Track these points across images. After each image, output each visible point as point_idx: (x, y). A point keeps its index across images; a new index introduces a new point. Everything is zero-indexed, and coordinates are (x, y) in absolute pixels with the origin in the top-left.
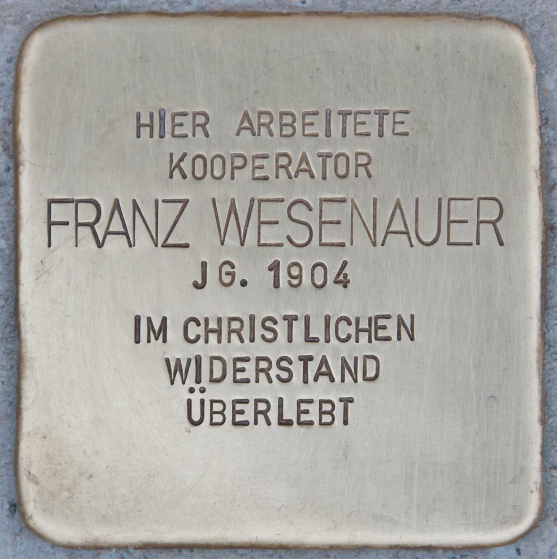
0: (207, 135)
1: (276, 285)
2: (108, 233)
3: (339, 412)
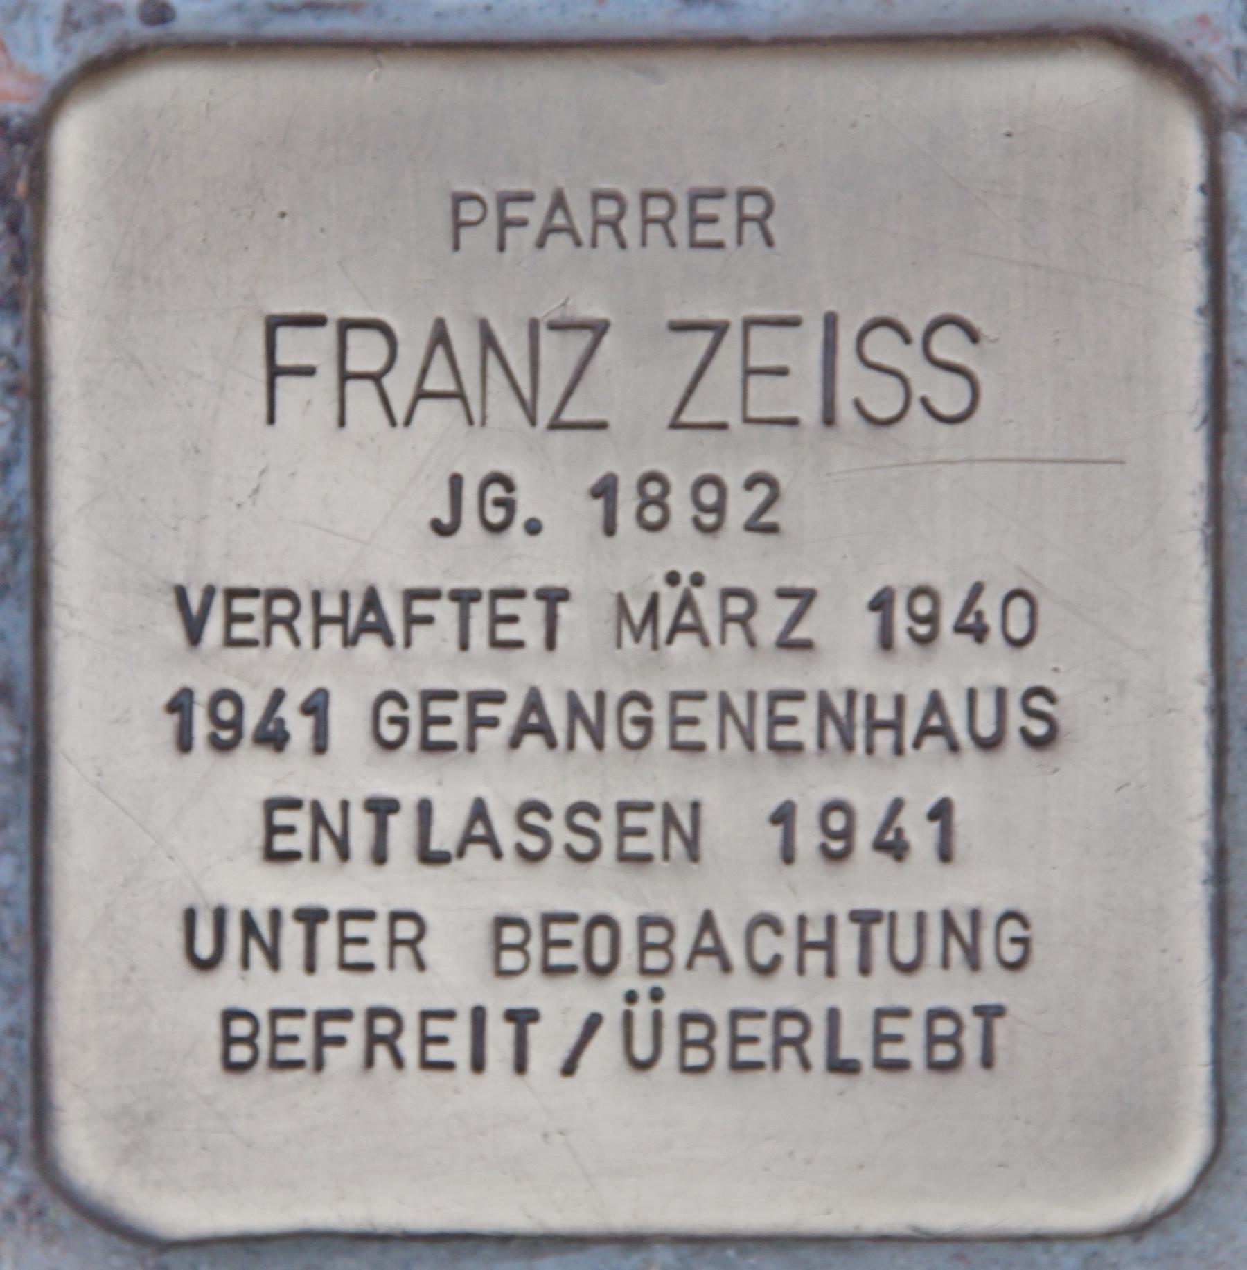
0: (769, 242)
1: (788, 856)
2: (421, 394)
3: (971, 1041)
